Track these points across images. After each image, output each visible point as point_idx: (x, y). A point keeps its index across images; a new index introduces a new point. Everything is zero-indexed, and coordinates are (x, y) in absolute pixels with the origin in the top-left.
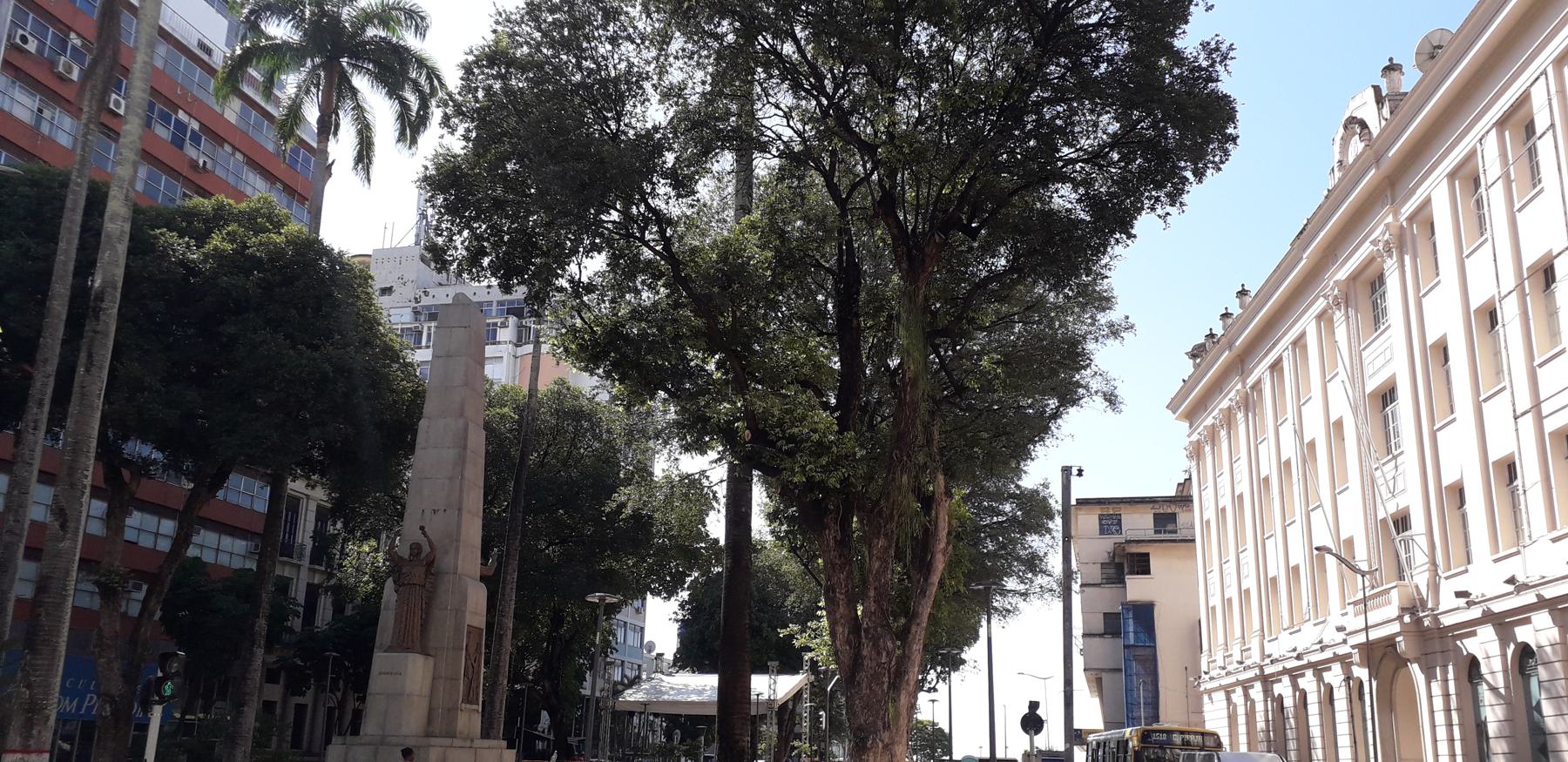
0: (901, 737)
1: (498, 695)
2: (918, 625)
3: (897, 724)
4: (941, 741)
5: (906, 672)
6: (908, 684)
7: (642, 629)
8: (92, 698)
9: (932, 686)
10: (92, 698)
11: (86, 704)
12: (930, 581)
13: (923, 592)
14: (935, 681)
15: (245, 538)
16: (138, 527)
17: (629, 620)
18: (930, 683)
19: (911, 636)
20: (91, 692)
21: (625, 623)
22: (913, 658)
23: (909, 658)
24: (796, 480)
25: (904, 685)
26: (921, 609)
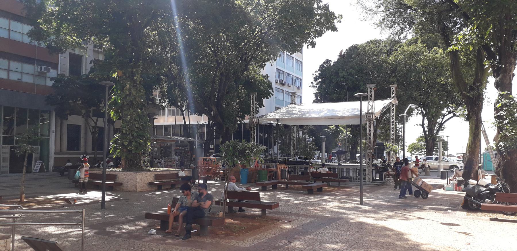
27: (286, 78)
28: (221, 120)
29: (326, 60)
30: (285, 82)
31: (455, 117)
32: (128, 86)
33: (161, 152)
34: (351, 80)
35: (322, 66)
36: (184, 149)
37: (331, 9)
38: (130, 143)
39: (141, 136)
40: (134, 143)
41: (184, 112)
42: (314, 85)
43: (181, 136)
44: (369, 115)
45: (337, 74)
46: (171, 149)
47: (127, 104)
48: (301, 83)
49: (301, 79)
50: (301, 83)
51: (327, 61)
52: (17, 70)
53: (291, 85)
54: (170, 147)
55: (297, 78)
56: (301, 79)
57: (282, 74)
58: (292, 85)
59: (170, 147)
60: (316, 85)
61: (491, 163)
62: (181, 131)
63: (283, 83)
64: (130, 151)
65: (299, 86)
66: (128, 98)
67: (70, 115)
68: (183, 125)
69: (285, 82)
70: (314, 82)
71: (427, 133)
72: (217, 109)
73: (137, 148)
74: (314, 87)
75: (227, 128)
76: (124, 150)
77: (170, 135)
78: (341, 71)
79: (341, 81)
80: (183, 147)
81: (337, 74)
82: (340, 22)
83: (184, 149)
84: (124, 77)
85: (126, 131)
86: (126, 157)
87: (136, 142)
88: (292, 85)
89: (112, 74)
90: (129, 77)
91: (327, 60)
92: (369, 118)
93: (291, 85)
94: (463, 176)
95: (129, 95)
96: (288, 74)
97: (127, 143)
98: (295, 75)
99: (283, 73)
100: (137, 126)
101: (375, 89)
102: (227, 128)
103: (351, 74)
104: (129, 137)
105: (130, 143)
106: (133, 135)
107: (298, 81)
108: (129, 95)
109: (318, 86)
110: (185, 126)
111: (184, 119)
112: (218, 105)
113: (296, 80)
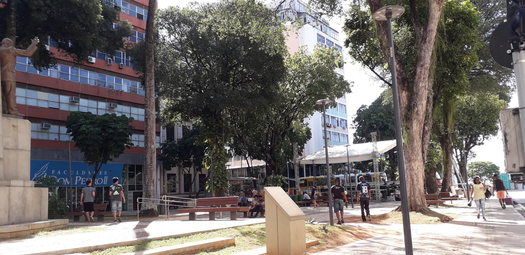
0: (417, 155)
1: (148, 154)
2: (422, 66)
3: (412, 146)
4: (494, 169)
5: (415, 105)
6: (418, 114)
7: (347, 135)
8: (78, 178)
9: (481, 142)
10: (78, 178)
11: (76, 181)
12: (428, 29)
13: (424, 40)
14: (482, 139)
15: (104, 101)
16: (137, 113)
17: (340, 132)
18: (480, 141)
19: (417, 77)
20: (77, 175)
21: (339, 133)
22: (420, 93)
23: (417, 94)
24: (422, 75)
25: (415, 116)
26: (423, 53)
27: (331, 121)
28: (274, 164)
29: (362, 105)
30: (331, 125)
31: (476, 146)
32: (215, 148)
33: (233, 189)
34: (382, 122)
35: (359, 111)
36: (249, 186)
37: (345, 79)
38: (218, 182)
39: (224, 178)
40: (220, 182)
41: (247, 159)
42: (353, 126)
43: (246, 177)
44: (374, 153)
45: (369, 117)
46: (240, 187)
47: (215, 159)
48: (346, 123)
49: (346, 120)
50: (346, 123)
51: (363, 106)
52: (136, 139)
53: (337, 127)
54: (239, 185)
55: (342, 120)
56: (346, 120)
57: (328, 118)
58: (338, 126)
59: (239, 185)
60: (355, 127)
61: (507, 183)
62: (245, 172)
63: (329, 125)
64: (218, 187)
65: (345, 126)
66: (215, 155)
67: (172, 167)
68: (247, 168)
69: (331, 125)
70: (353, 124)
71: (460, 160)
72: (271, 156)
73: (222, 185)
74: (353, 128)
75: (278, 168)
76: (215, 187)
77: (244, 177)
78: (372, 114)
79: (372, 123)
80: (249, 185)
81: (369, 117)
82: (353, 86)
83: (249, 186)
84: (212, 142)
85: (215, 175)
86: (216, 191)
87: (221, 181)
88: (338, 126)
89: (205, 141)
90: (215, 142)
91: (363, 105)
92: (374, 155)
93: (337, 127)
94: (190, 167)
95: (216, 153)
96: (333, 118)
97: (216, 182)
98: (340, 117)
99: (329, 117)
100: (221, 172)
101: (376, 135)
102: (278, 168)
103: (381, 117)
104: (217, 179)
105: (218, 182)
106: (219, 178)
107: (343, 122)
108: (216, 153)
109: (357, 127)
110: (248, 169)
111: (248, 163)
112: (271, 152)
113: (342, 121)
